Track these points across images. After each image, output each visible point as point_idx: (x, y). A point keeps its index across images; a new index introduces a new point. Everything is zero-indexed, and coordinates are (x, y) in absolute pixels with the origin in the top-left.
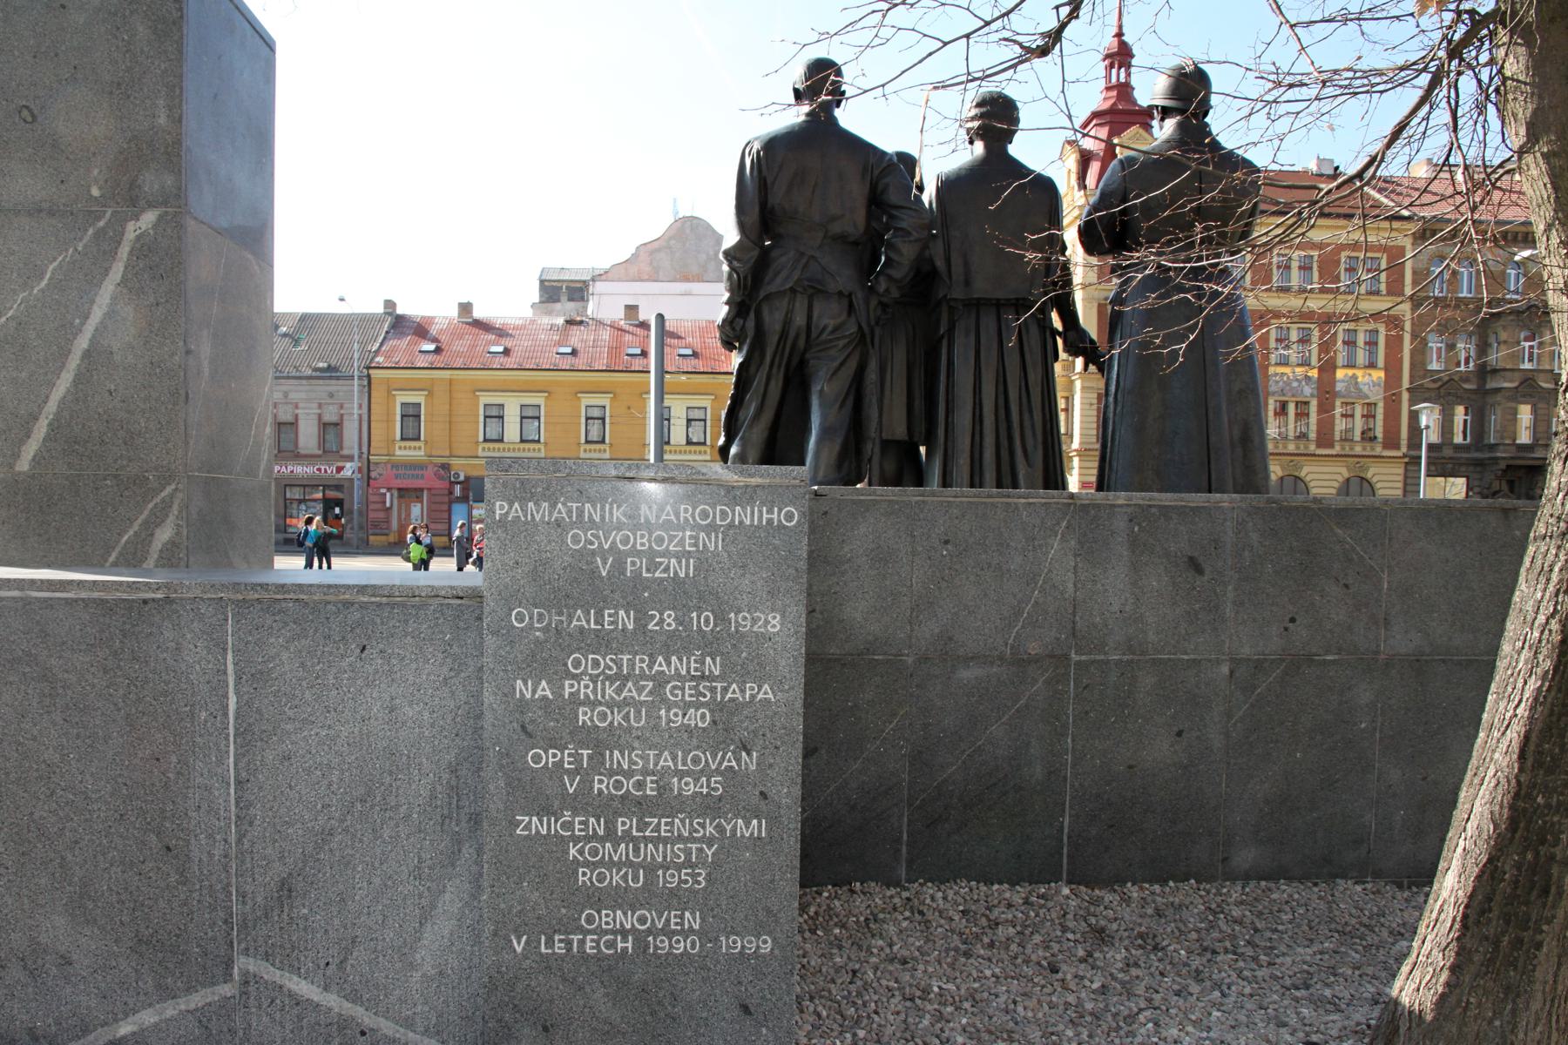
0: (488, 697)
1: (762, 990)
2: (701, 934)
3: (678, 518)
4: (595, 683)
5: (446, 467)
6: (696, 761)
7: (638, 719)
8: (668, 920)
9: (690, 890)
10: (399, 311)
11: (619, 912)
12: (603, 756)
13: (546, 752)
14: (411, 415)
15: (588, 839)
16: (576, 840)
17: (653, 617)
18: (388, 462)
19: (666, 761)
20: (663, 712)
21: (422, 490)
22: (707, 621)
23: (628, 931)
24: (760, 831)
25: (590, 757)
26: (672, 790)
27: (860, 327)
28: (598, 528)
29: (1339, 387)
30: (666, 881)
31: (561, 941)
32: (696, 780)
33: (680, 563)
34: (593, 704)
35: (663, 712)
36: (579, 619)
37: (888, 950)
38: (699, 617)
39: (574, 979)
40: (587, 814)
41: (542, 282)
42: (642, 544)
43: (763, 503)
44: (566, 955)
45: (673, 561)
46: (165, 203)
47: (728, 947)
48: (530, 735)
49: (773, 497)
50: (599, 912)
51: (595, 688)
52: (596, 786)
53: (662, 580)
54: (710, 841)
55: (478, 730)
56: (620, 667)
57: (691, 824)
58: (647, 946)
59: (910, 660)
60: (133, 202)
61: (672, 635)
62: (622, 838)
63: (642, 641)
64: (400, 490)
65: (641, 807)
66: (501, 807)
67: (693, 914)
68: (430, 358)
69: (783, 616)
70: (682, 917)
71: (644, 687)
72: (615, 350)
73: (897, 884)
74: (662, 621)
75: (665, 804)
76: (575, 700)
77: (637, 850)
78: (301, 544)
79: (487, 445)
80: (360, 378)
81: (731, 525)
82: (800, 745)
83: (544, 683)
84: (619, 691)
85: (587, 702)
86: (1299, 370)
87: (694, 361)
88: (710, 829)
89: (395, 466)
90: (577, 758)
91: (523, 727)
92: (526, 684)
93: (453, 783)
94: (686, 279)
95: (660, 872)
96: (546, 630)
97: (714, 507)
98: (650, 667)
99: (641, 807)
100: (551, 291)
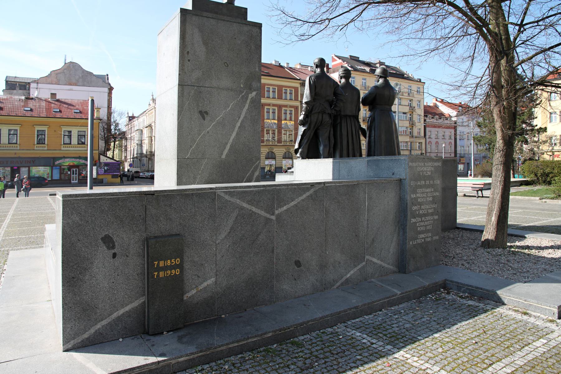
29: (283, 126)
46: (258, 90)
60: (250, 89)
65: (425, 215)
72: (48, 109)
86: (272, 121)
87: (80, 115)
94: (70, 85)
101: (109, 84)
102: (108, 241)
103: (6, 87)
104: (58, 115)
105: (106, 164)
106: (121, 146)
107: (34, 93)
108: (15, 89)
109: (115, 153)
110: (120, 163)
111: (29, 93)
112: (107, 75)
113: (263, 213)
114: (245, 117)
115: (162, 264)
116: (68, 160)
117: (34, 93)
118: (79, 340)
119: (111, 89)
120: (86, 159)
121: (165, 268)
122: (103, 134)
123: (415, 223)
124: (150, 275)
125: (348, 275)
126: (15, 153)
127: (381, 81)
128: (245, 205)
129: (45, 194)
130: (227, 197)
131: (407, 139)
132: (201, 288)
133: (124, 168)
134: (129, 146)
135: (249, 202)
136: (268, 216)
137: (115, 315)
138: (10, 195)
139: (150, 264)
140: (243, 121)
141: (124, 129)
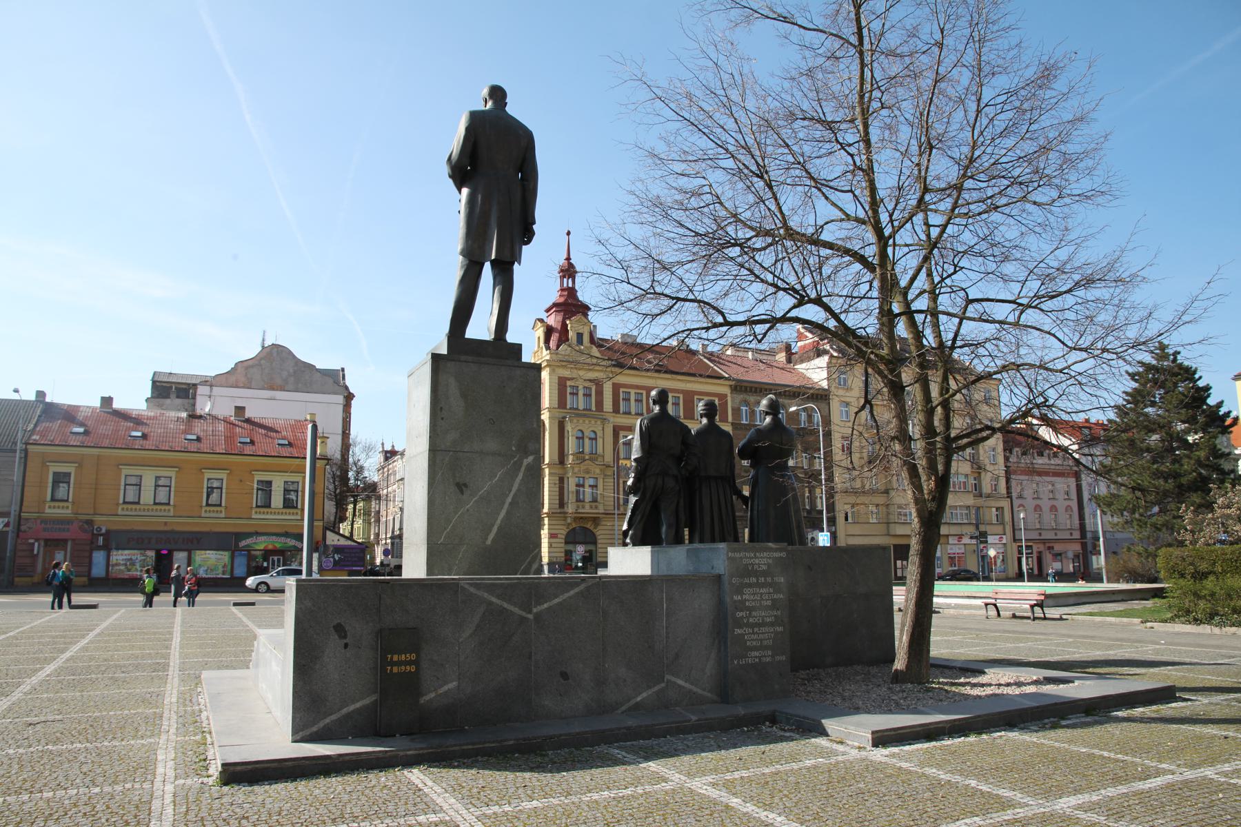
5: (90, 523)
10: (48, 400)
18: (38, 518)
21: (65, 541)
41: (154, 382)
63: (758, 585)
64: (46, 541)
65: (759, 625)
72: (230, 438)
75: (763, 624)
78: (49, 583)
79: (125, 506)
87: (290, 449)
89: (45, 521)
94: (272, 388)
99: (759, 625)
100: (164, 389)
101: (347, 388)
102: (340, 630)
103: (153, 392)
104: (248, 449)
105: (338, 549)
106: (367, 513)
107: (205, 405)
108: (167, 397)
109: (355, 526)
110: (364, 549)
111: (194, 405)
112: (343, 370)
113: (516, 610)
114: (519, 490)
115: (395, 658)
116: (263, 538)
117: (205, 406)
118: (307, 732)
119: (349, 397)
120: (299, 537)
121: (399, 663)
122: (331, 487)
123: (743, 635)
124: (383, 669)
125: (639, 699)
126: (166, 523)
127: (768, 419)
128: (494, 600)
129: (226, 603)
130: (472, 590)
131: (970, 500)
132: (441, 691)
133: (373, 558)
134: (383, 513)
135: (498, 597)
136: (524, 614)
137: (345, 711)
138: (163, 604)
139: (384, 658)
140: (515, 495)
141: (372, 475)
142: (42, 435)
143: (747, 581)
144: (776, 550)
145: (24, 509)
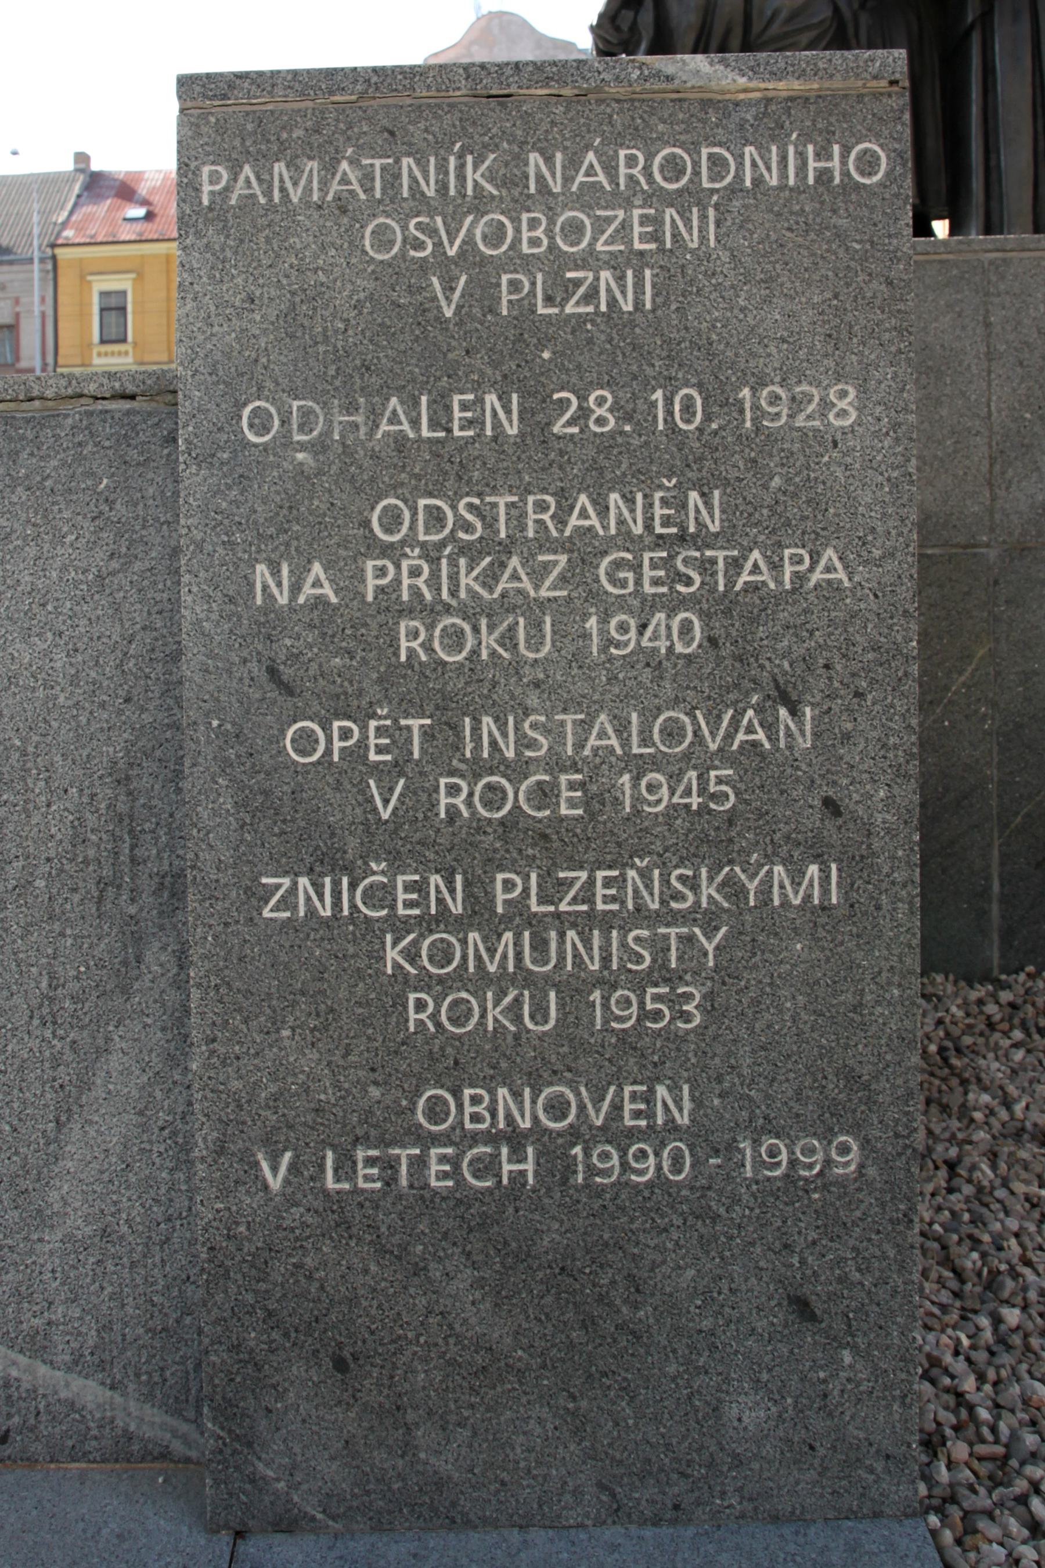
0: (192, 608)
1: (840, 1261)
2: (698, 1135)
3: (613, 179)
4: (434, 561)
6: (673, 732)
7: (535, 641)
8: (617, 1107)
9: (668, 1035)
10: (95, 166)
11: (502, 1092)
12: (456, 729)
13: (326, 728)
14: (114, 308)
15: (427, 924)
16: (399, 927)
17: (564, 404)
19: (602, 736)
20: (592, 623)
22: (688, 408)
23: (526, 1135)
24: (825, 891)
25: (427, 734)
26: (617, 802)
27: (836, 10)
28: (431, 213)
30: (609, 1016)
31: (370, 1162)
32: (675, 778)
33: (621, 279)
34: (431, 612)
35: (592, 623)
36: (394, 419)
37: (1004, 1115)
38: (669, 401)
39: (404, 1248)
40: (424, 866)
42: (534, 242)
43: (806, 137)
44: (384, 1193)
45: (605, 275)
47: (759, 1164)
48: (288, 689)
49: (825, 119)
50: (457, 1093)
51: (435, 575)
52: (444, 800)
53: (582, 319)
54: (710, 921)
55: (171, 688)
56: (490, 524)
57: (666, 881)
58: (570, 1169)
59: (993, 554)
61: (607, 444)
62: (506, 920)
63: (539, 458)
65: (548, 845)
66: (227, 856)
67: (674, 1089)
68: (138, 227)
69: (862, 390)
70: (649, 1098)
71: (547, 567)
73: (986, 978)
74: (584, 413)
75: (605, 836)
76: (391, 606)
77: (540, 946)
80: (42, 260)
81: (735, 189)
82: (911, 686)
83: (317, 568)
84: (489, 579)
85: (417, 607)
88: (708, 891)
90: (398, 737)
91: (273, 672)
92: (276, 573)
93: (122, 807)
95: (596, 996)
96: (319, 447)
97: (693, 150)
98: (561, 521)
142: (79, 230)
143: (401, 420)
144: (770, 121)
145: (60, 361)
